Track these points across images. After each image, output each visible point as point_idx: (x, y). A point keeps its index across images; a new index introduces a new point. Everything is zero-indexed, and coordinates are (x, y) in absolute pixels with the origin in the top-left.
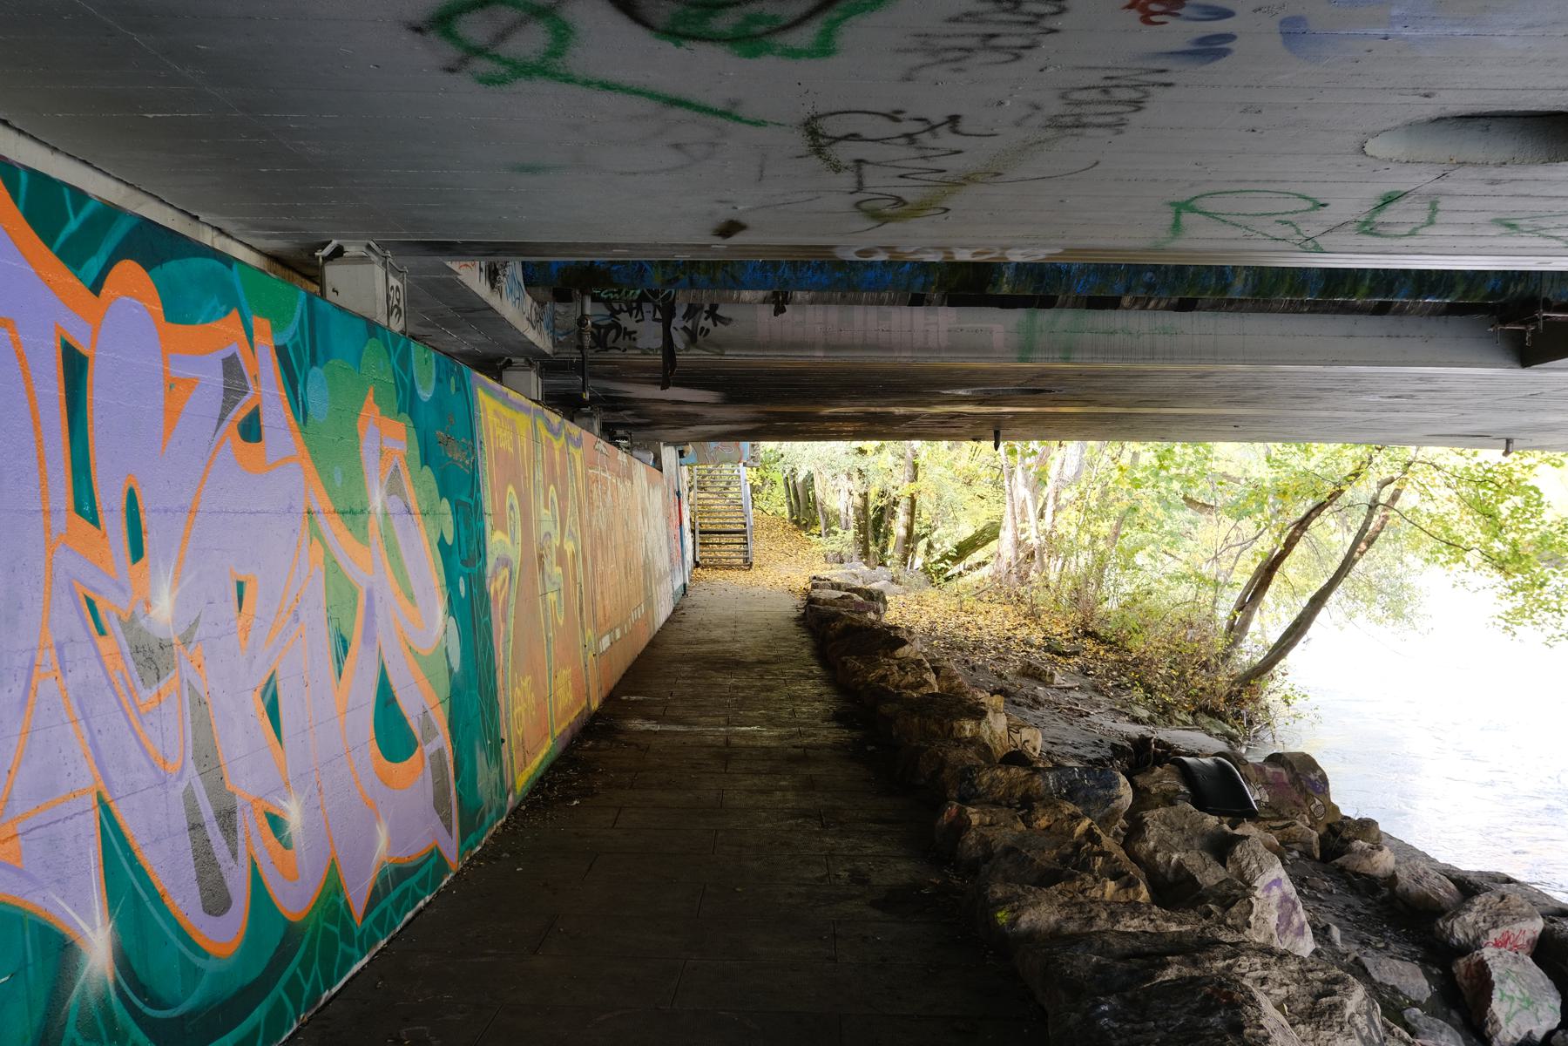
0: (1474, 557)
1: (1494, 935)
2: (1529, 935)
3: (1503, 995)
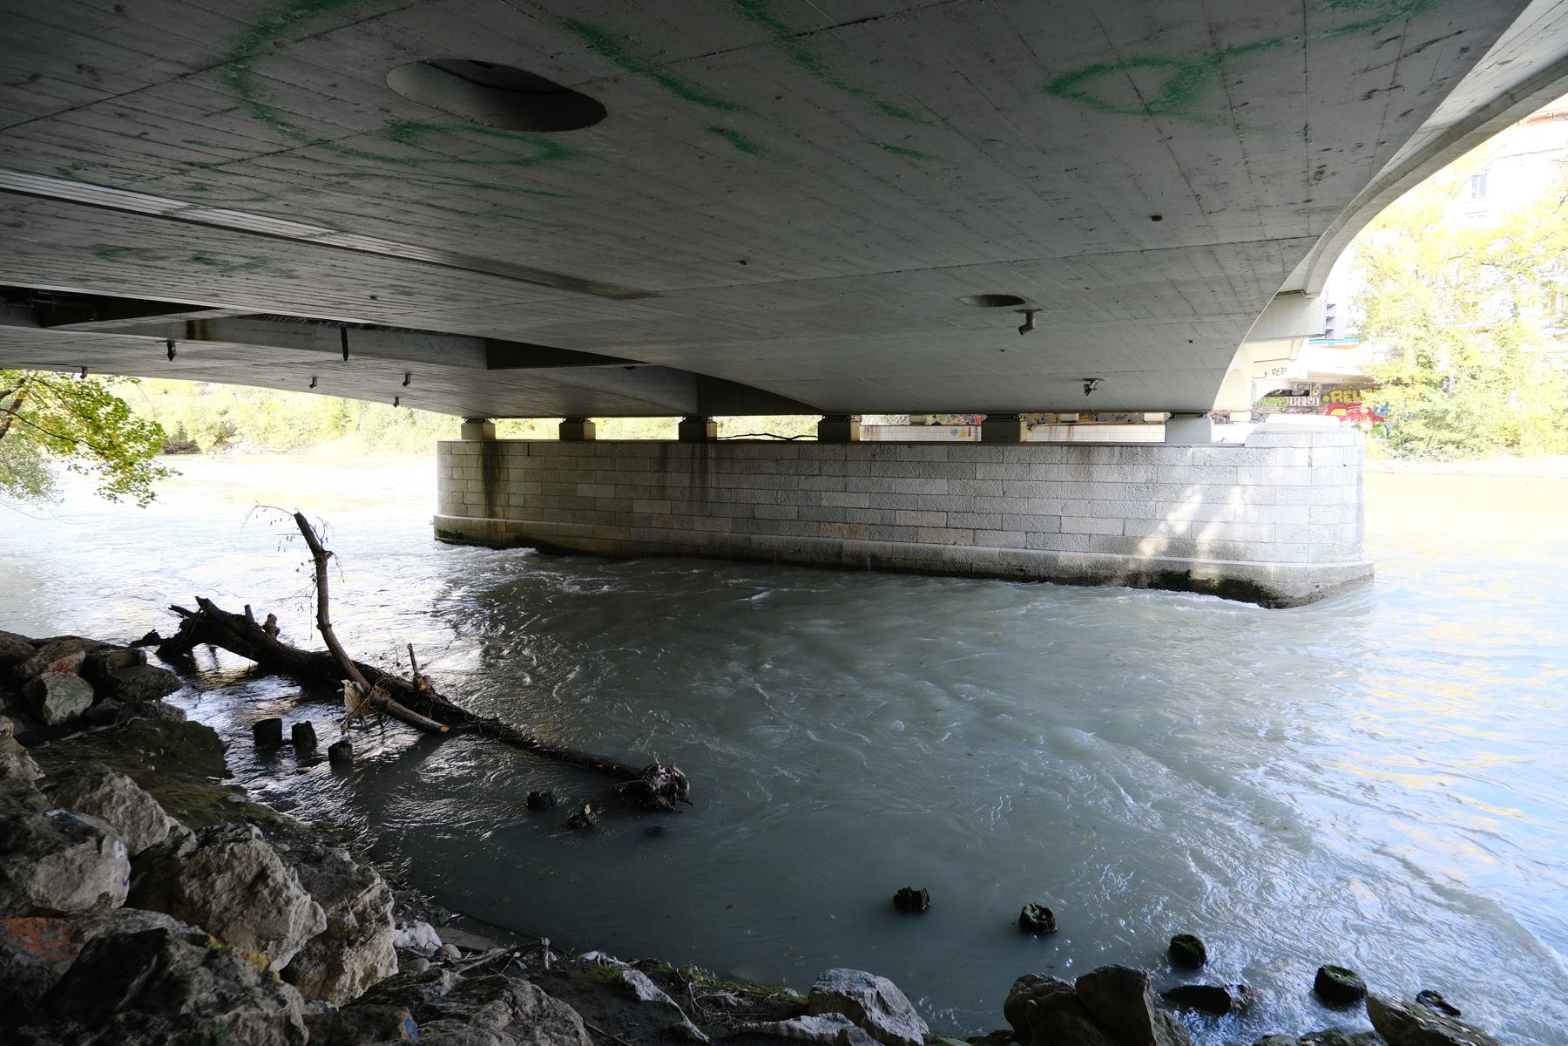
0: (83, 448)
1: (51, 666)
2: (76, 662)
3: (53, 695)
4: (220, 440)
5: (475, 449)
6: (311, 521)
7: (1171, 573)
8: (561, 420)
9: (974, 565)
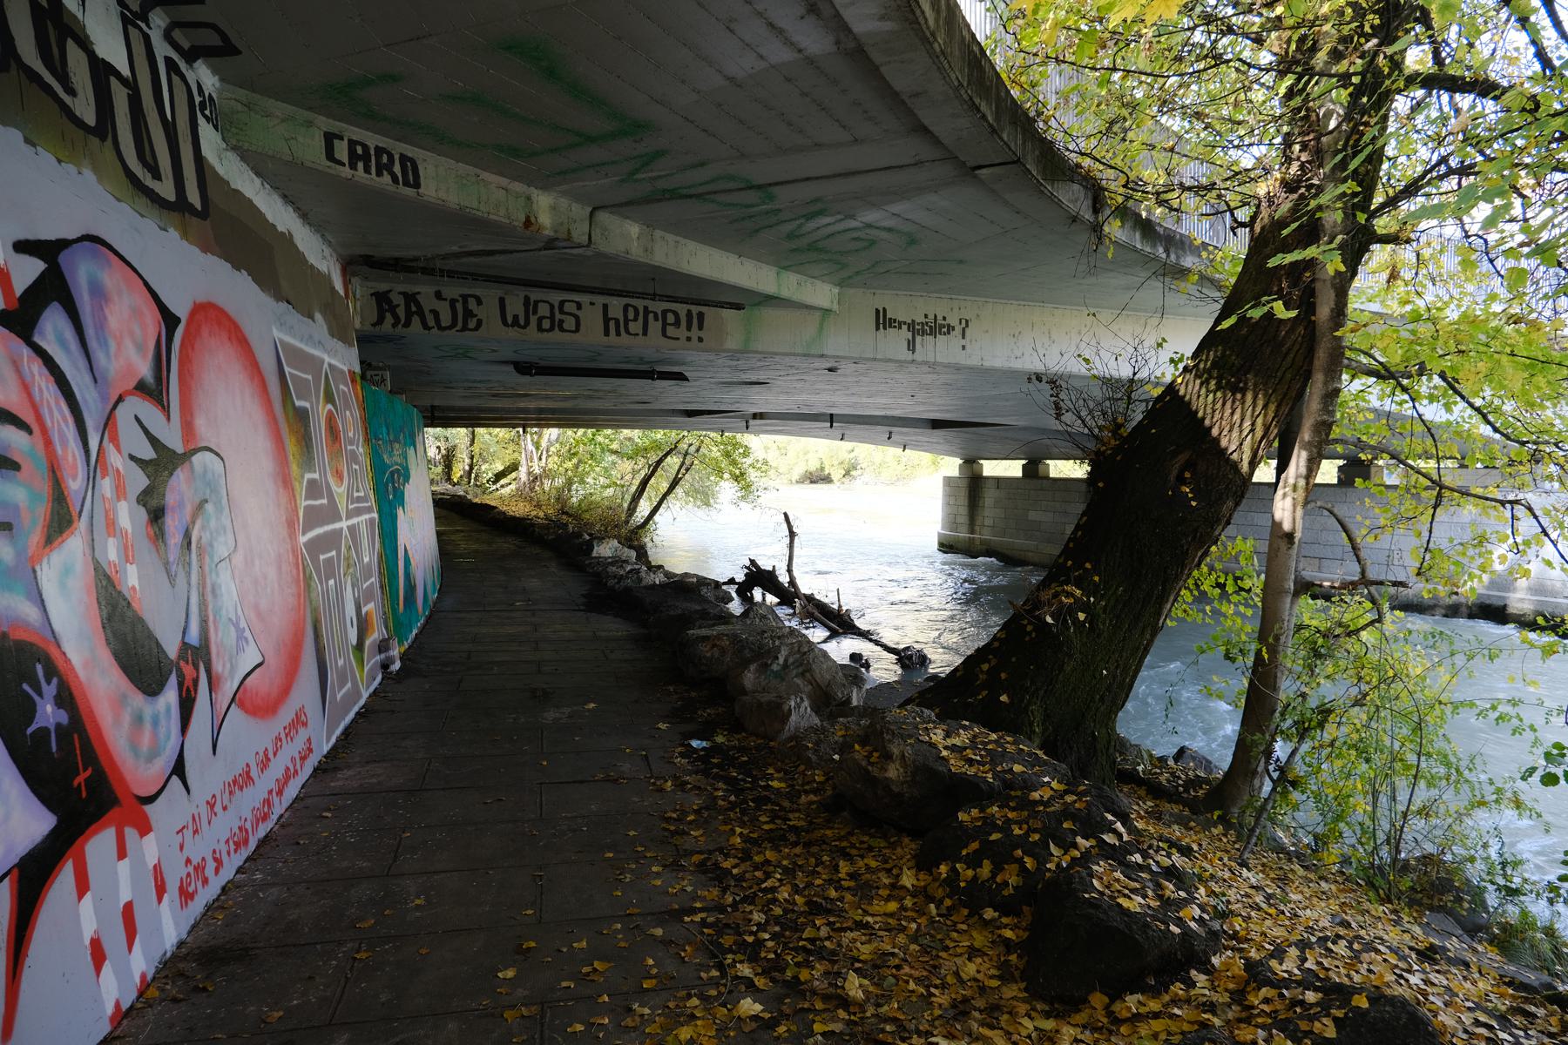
4: (847, 473)
5: (964, 483)
6: (791, 518)
7: (1489, 606)
8: (1024, 462)
9: (727, 490)
